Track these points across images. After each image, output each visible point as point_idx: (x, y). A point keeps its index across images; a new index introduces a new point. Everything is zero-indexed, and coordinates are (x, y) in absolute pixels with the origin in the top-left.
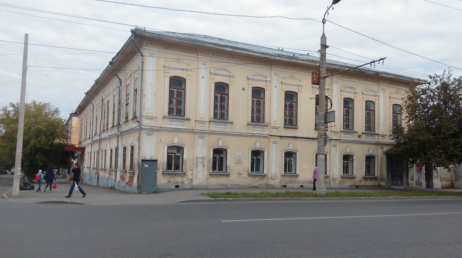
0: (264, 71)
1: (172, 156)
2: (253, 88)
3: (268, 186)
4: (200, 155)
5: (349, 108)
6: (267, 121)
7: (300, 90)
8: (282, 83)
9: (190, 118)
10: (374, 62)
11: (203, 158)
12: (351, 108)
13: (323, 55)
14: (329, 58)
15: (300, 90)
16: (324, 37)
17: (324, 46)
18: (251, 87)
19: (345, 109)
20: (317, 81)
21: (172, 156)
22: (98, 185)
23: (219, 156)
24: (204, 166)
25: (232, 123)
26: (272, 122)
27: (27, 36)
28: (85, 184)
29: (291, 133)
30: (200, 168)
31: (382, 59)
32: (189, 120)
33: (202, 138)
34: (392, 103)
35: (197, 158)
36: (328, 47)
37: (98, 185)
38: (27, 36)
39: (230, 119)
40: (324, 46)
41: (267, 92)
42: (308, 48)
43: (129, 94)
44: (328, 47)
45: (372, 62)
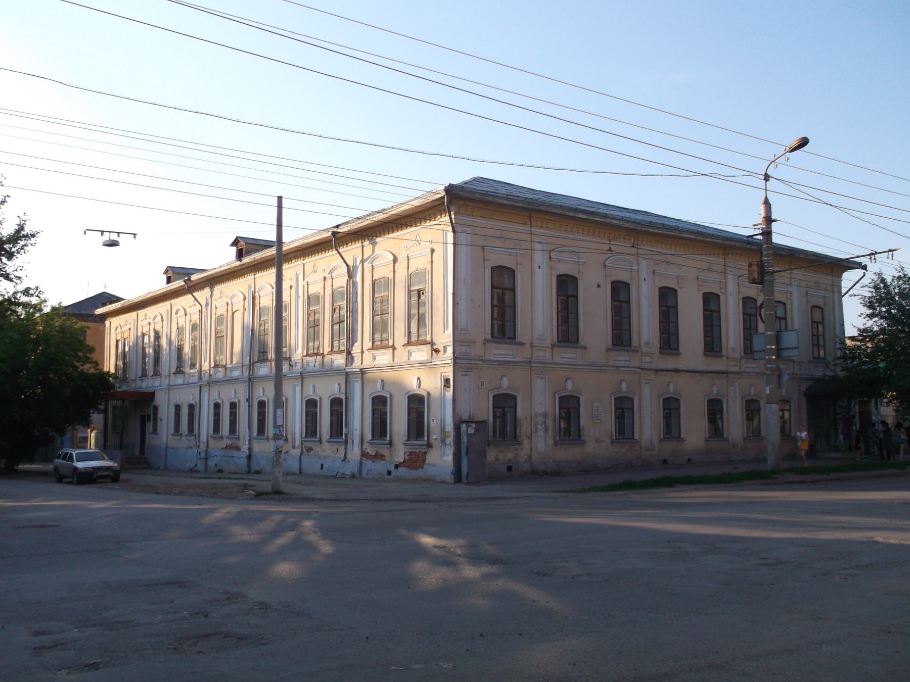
0: (518, 230)
1: (115, 407)
2: (558, 276)
3: (428, 480)
4: (540, 409)
5: (668, 307)
6: (635, 343)
7: (680, 286)
8: (654, 272)
9: (524, 341)
10: (876, 253)
11: (545, 415)
12: (571, 296)
13: (767, 233)
14: (776, 239)
15: (680, 286)
16: (767, 203)
17: (769, 220)
18: (609, 280)
19: (560, 298)
20: (762, 277)
21: (115, 407)
22: (300, 472)
23: (569, 408)
24: (546, 430)
25: (585, 348)
26: (643, 344)
27: (280, 199)
28: (257, 472)
29: (670, 363)
30: (541, 433)
31: (890, 251)
32: (522, 344)
33: (542, 378)
34: (810, 305)
35: (536, 415)
36: (775, 221)
37: (300, 472)
38: (280, 199)
39: (582, 342)
40: (769, 220)
41: (633, 289)
42: (743, 222)
43: (172, 273)
44: (775, 221)
45: (872, 254)
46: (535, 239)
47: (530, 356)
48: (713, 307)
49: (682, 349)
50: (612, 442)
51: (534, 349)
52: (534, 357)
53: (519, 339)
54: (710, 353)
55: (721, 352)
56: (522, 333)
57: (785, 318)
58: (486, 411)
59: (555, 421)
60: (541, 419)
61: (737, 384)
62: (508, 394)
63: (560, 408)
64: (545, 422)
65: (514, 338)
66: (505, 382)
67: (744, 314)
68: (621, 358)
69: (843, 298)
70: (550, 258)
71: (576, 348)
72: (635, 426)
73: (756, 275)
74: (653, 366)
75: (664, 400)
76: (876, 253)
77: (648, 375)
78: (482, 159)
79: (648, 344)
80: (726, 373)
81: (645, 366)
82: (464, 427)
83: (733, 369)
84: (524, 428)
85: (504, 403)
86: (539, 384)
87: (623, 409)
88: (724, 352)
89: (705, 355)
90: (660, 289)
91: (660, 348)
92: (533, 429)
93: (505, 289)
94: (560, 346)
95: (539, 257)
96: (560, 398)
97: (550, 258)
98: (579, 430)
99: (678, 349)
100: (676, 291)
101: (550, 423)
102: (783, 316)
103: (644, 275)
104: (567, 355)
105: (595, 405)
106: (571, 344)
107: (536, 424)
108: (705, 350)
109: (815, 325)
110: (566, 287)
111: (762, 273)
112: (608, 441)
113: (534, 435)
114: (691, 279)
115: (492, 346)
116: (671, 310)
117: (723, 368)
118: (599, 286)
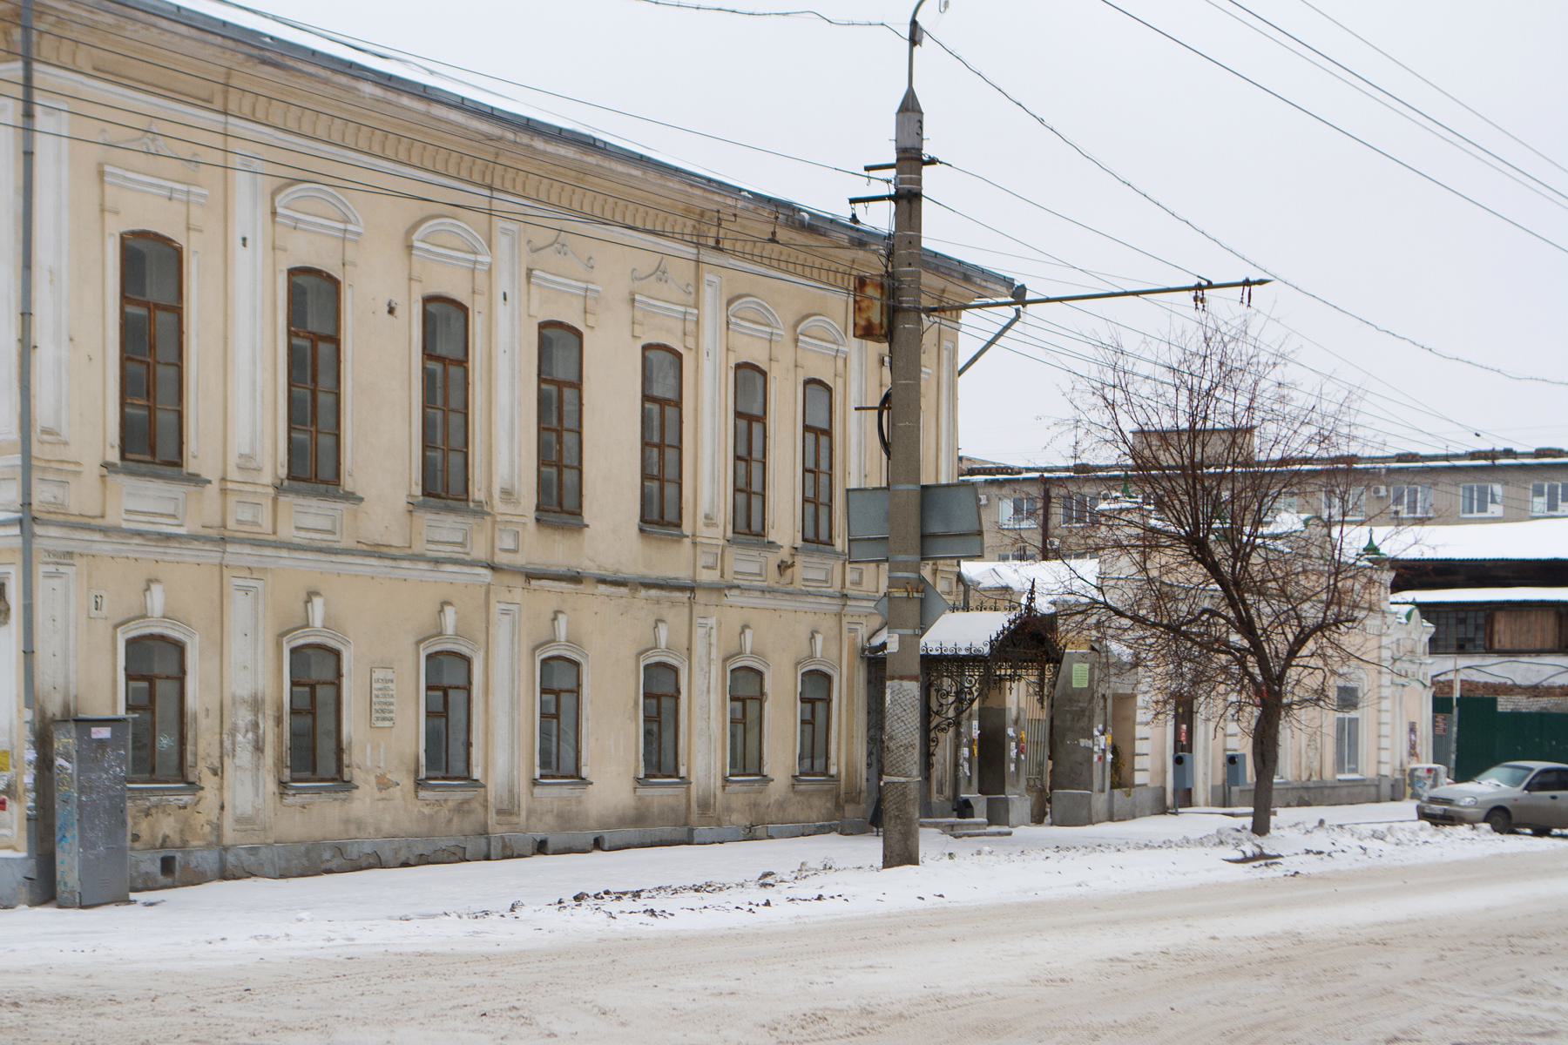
6: (477, 492)
7: (591, 320)
9: (205, 476)
10: (1210, 285)
11: (256, 704)
16: (910, 108)
17: (911, 158)
24: (258, 748)
25: (352, 497)
29: (556, 551)
30: (245, 756)
32: (196, 480)
39: (348, 483)
40: (911, 158)
41: (477, 325)
46: (233, 145)
47: (217, 521)
48: (562, 371)
49: (587, 516)
50: (419, 784)
51: (232, 499)
52: (231, 524)
53: (191, 466)
54: (656, 529)
55: (679, 525)
56: (200, 451)
57: (828, 433)
58: (104, 690)
59: (279, 721)
60: (244, 717)
61: (712, 621)
62: (162, 638)
63: (294, 684)
64: (256, 725)
65: (178, 463)
66: (157, 600)
67: (646, 397)
68: (445, 528)
69: (962, 380)
70: (274, 213)
71: (172, 479)
72: (474, 740)
73: (876, 316)
74: (519, 560)
75: (131, 643)
76: (1210, 285)
77: (509, 589)
78: (1231, 246)
79: (507, 493)
80: (691, 588)
81: (502, 559)
82: (64, 741)
83: (707, 576)
84: (204, 742)
85: (154, 663)
86: (240, 609)
87: (151, 680)
88: (687, 528)
89: (642, 530)
90: (543, 326)
91: (538, 509)
92: (227, 744)
93: (158, 306)
94: (297, 492)
95: (247, 211)
96: (293, 651)
97: (274, 213)
98: (339, 751)
99: (577, 512)
100: (579, 335)
101: (268, 727)
102: (671, 395)
103: (503, 283)
104: (309, 521)
105: (378, 674)
106: (322, 487)
107: (234, 731)
108: (643, 519)
109: (655, 408)
110: (312, 303)
111: (893, 312)
112: (407, 783)
113: (227, 761)
114: (624, 304)
115: (425, 518)
116: (161, 316)
117: (682, 573)
118: (391, 311)
